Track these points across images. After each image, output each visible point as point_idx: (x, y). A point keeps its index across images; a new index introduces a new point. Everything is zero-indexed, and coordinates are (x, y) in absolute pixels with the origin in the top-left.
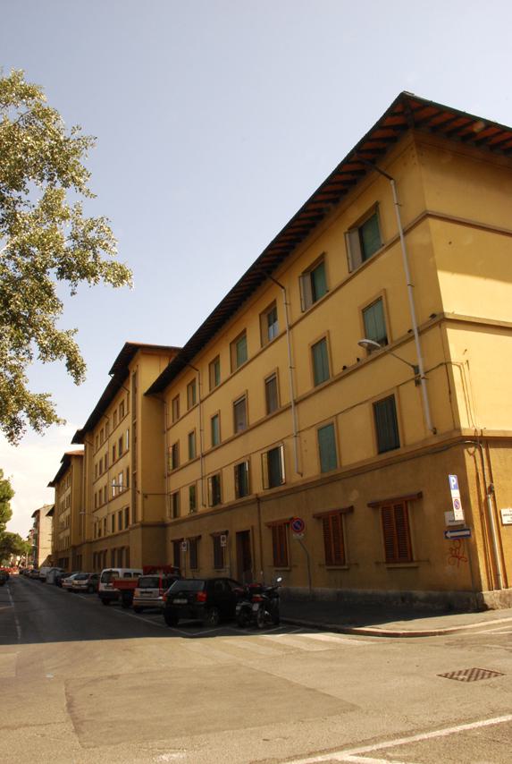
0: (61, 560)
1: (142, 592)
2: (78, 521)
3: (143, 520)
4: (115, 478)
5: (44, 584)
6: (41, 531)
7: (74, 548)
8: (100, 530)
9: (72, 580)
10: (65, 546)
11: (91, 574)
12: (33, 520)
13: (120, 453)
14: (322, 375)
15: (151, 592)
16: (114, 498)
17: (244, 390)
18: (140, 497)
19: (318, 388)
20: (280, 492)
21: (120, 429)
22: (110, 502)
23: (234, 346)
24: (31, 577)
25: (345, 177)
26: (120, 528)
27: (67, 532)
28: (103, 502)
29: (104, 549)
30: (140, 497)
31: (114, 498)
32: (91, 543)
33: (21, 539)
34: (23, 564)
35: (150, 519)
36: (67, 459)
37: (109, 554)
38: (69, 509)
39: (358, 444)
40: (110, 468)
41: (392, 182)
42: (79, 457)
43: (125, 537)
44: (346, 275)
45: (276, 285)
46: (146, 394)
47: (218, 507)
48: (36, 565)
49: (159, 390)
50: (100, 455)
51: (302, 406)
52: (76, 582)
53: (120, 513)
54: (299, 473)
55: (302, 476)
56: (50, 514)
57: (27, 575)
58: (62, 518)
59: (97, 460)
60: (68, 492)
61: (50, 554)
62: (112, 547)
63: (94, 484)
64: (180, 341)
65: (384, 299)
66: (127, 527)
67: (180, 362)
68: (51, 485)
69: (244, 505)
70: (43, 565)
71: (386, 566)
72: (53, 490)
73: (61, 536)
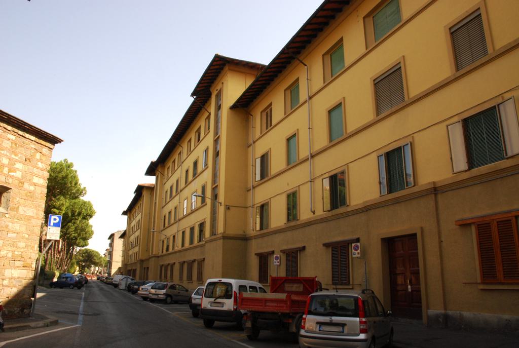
0: (129, 271)
1: (320, 324)
2: (148, 234)
3: (224, 232)
4: (187, 198)
5: (116, 289)
6: (114, 249)
7: (142, 261)
8: (168, 247)
9: (147, 288)
10: (133, 260)
11: (170, 284)
12: (109, 241)
13: (194, 174)
14: (337, 133)
15: (343, 325)
16: (185, 217)
17: (296, 129)
18: (221, 210)
19: (290, 166)
20: (264, 233)
21: (197, 152)
22: (179, 220)
23: (328, 58)
24: (105, 283)
25: (321, 20)
26: (192, 242)
27: (136, 249)
28: (172, 221)
29: (172, 262)
30: (221, 210)
31: (185, 217)
32: (158, 257)
33: (99, 254)
34: (100, 273)
35: (231, 232)
36: (140, 190)
37: (177, 267)
38: (139, 230)
39: (365, 186)
40: (181, 191)
41: (306, 67)
42: (151, 189)
43: (198, 250)
44: (283, 116)
45: (301, 63)
46: (234, 107)
47: (341, 210)
48: (109, 274)
49: (244, 105)
50: (167, 187)
51: (317, 159)
52: (153, 291)
53: (192, 229)
54: (312, 212)
55: (314, 214)
56: (123, 236)
57: (102, 281)
58: (132, 238)
59: (167, 187)
60: (139, 217)
61: (121, 266)
62: (181, 260)
63: (163, 207)
64: (265, 56)
65: (343, 103)
66: (200, 240)
67: (265, 78)
68: (125, 213)
69: (397, 201)
70: (116, 273)
71: (481, 287)
72: (126, 217)
73: (131, 252)
